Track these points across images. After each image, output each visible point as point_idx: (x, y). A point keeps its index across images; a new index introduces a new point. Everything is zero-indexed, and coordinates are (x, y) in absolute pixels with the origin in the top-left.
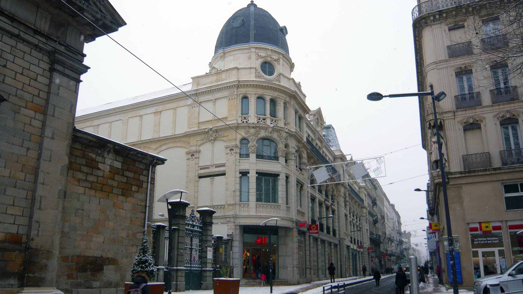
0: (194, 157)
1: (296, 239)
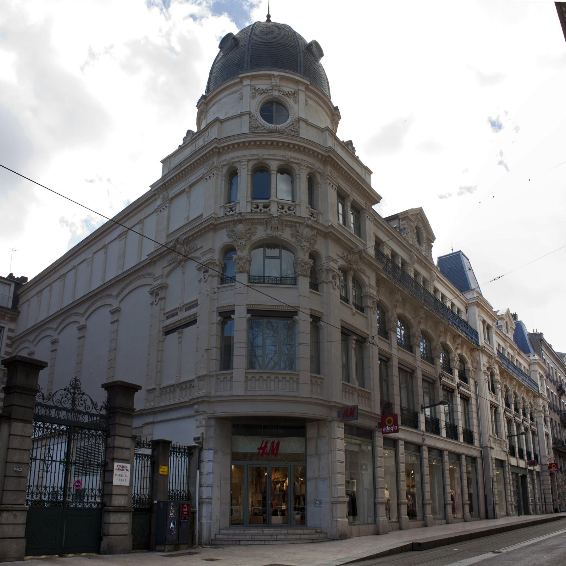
1: (340, 444)
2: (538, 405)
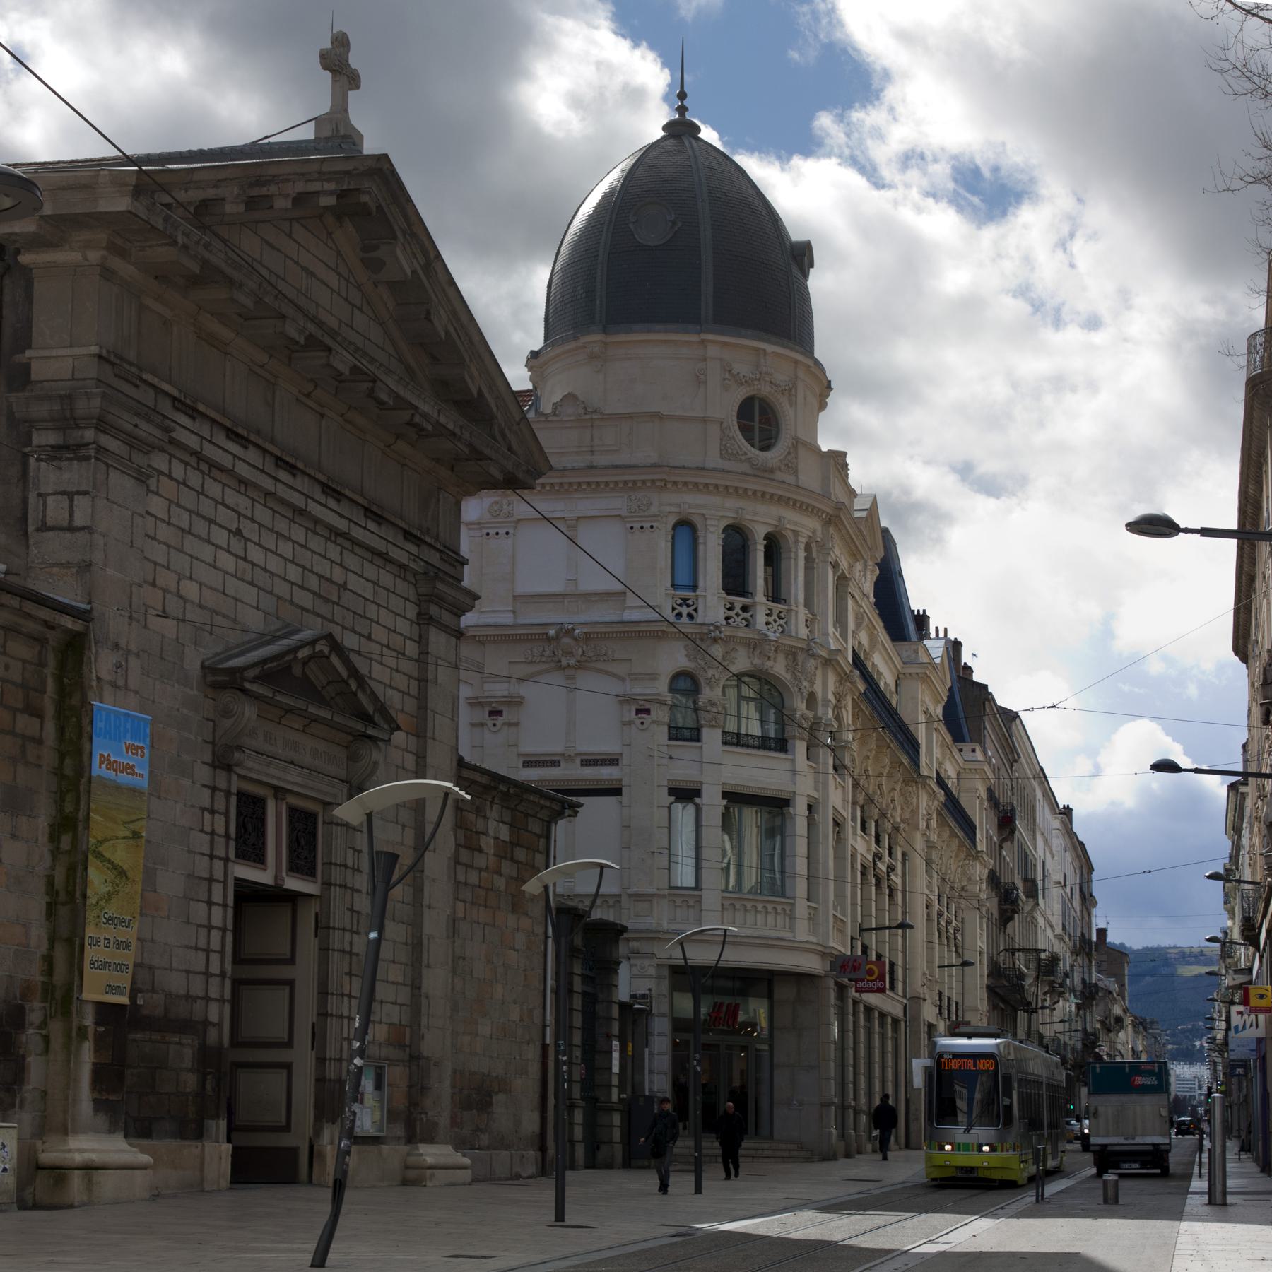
0: (500, 721)
2: (970, 879)
